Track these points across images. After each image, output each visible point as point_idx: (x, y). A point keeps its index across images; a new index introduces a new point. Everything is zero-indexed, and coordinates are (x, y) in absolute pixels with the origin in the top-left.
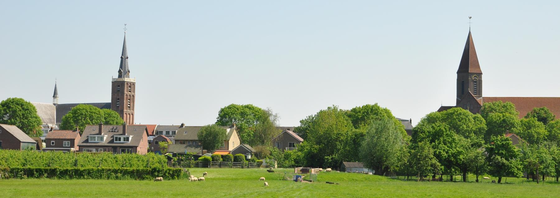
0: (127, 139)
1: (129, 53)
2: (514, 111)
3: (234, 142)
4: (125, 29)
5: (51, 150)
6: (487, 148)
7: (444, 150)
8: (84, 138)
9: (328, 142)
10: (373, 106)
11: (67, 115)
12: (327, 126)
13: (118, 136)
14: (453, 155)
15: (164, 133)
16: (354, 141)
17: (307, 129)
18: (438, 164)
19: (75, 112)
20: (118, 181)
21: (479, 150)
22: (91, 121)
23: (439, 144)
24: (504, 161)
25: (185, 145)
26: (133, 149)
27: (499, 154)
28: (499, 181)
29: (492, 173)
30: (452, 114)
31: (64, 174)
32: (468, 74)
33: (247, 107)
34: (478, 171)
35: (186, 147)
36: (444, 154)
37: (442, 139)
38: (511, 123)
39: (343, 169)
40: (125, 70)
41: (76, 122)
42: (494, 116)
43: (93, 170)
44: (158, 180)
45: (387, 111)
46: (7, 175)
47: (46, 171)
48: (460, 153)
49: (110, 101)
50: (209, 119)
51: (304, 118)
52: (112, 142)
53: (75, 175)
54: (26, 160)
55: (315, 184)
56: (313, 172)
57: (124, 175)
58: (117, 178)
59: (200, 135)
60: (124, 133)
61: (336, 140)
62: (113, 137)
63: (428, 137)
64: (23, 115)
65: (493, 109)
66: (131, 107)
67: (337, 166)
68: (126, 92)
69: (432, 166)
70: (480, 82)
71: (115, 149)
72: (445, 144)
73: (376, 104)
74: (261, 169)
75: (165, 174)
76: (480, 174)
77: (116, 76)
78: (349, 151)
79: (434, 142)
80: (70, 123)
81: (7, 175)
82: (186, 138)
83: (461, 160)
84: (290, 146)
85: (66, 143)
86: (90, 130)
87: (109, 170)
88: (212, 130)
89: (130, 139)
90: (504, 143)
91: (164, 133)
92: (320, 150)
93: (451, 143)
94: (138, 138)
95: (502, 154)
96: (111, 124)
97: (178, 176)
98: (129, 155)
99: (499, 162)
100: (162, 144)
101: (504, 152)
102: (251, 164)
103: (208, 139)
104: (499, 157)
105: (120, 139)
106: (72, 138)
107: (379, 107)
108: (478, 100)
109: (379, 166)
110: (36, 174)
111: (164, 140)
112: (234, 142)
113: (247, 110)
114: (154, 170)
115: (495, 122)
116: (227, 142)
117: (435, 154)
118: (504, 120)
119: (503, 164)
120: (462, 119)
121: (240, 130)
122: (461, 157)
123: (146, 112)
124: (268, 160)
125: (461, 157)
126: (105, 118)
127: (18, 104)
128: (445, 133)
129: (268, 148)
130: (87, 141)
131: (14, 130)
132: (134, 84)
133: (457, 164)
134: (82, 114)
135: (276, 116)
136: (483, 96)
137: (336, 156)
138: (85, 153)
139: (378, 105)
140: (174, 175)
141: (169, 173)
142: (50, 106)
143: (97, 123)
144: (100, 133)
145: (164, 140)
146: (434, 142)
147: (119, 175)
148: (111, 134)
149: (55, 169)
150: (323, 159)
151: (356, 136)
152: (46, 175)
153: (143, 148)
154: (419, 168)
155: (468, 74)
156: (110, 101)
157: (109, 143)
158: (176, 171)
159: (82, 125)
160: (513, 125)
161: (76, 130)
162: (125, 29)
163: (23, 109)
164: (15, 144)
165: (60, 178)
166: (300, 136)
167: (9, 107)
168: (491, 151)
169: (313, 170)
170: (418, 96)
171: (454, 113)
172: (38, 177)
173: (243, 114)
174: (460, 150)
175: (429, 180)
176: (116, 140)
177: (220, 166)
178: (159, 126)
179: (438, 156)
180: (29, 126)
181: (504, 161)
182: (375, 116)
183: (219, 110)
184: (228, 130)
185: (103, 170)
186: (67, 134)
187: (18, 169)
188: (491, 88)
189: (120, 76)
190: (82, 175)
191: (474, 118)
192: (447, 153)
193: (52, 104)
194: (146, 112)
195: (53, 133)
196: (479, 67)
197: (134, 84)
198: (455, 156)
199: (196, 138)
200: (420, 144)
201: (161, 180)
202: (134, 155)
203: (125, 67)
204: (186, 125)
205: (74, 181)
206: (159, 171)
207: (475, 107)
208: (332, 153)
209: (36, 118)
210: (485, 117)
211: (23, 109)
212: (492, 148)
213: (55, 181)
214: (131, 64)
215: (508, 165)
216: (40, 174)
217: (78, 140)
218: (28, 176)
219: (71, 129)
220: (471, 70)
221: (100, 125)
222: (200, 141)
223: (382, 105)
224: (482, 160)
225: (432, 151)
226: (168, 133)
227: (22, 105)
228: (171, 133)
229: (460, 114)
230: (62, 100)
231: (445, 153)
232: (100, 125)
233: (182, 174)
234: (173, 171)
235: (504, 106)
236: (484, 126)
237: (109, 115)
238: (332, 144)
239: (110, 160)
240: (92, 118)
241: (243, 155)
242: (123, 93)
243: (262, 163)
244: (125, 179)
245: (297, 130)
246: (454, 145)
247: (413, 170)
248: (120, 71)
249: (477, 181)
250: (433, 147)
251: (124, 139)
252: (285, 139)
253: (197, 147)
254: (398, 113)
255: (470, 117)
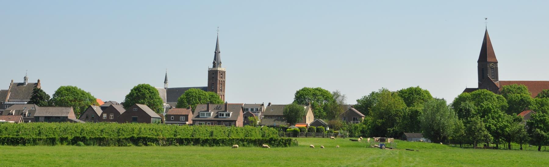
0: (229, 115)
1: (221, 49)
2: (527, 92)
3: (310, 119)
4: (218, 31)
5: (172, 123)
6: (527, 122)
7: (493, 124)
8: (196, 114)
9: (389, 117)
10: (416, 88)
11: (182, 96)
12: (386, 105)
13: (222, 113)
14: (500, 127)
15: (250, 110)
16: (411, 116)
17: (365, 106)
18: (490, 135)
19: (187, 94)
20: (245, 148)
21: (520, 124)
22: (200, 101)
23: (489, 118)
24: (543, 133)
25: (273, 120)
26: (232, 122)
27: (538, 127)
28: (539, 149)
29: (532, 143)
30: (479, 94)
31: (205, 142)
32: (486, 62)
33: (317, 89)
34: (521, 141)
35: (275, 121)
36: (493, 127)
37: (490, 115)
38: (528, 102)
39: (405, 139)
40: (218, 62)
41: (189, 102)
42: (514, 96)
43: (226, 139)
44: (264, 147)
45: (427, 92)
46: (165, 143)
47: (192, 140)
48: (506, 126)
49: (207, 86)
50: (289, 100)
51: (360, 97)
52: (217, 117)
53: (213, 143)
54: (176, 131)
55: (394, 150)
56: (389, 142)
57: (248, 144)
58: (244, 145)
59: (285, 112)
60: (226, 111)
61: (396, 115)
62: (218, 113)
63: (479, 113)
64: (150, 96)
65: (510, 90)
66: (223, 90)
67: (399, 136)
68: (218, 78)
69: (484, 136)
70: (497, 68)
71: (219, 122)
72: (493, 119)
73: (418, 87)
74: (346, 139)
75: (279, 143)
76: (523, 143)
77: (211, 66)
78: (406, 124)
79: (484, 117)
80: (184, 102)
81: (165, 143)
82: (273, 114)
83: (507, 132)
84: (354, 120)
85: (182, 118)
86: (200, 108)
87: (238, 139)
88: (294, 107)
89: (231, 114)
90: (542, 118)
91: (250, 110)
92: (383, 123)
93: (497, 118)
94: (236, 114)
95: (541, 127)
96: (214, 103)
97: (289, 144)
98: (229, 128)
99: (539, 134)
100: (250, 118)
101: (542, 126)
102: (329, 135)
103: (291, 115)
104: (538, 130)
105: (223, 115)
106: (186, 114)
107: (421, 89)
108: (496, 83)
109: (436, 135)
110: (185, 142)
111: (252, 115)
112: (310, 119)
113: (317, 92)
114: (271, 139)
115: (515, 101)
116: (305, 117)
117: (486, 127)
118: (522, 100)
119: (542, 135)
120: (488, 98)
121: (313, 107)
122: (507, 129)
123: (233, 94)
124: (342, 131)
125: (507, 129)
126: (210, 99)
127: (146, 89)
128: (493, 110)
129: (338, 121)
130: (198, 116)
131: (144, 108)
132: (224, 72)
133: (503, 135)
134: (193, 96)
135: (343, 97)
136: (500, 79)
137: (396, 128)
138: (197, 126)
139: (420, 87)
140: (286, 143)
141: (282, 142)
142: (162, 89)
143: (204, 103)
144: (208, 110)
145: (252, 115)
146: (484, 117)
147: (245, 143)
148: (217, 111)
149: (199, 139)
150: (386, 131)
151: (412, 112)
152: (192, 143)
153: (240, 122)
154: (474, 138)
155: (486, 62)
156: (207, 86)
157: (215, 117)
158: (288, 140)
159: (194, 104)
160: (529, 103)
161: (189, 108)
162: (218, 31)
163: (150, 92)
164: (147, 119)
165: (202, 145)
166: (359, 111)
167: (140, 91)
168: (530, 125)
169: (389, 139)
170: (450, 81)
171: (481, 94)
172: (186, 145)
173: (314, 95)
174: (506, 124)
175: (481, 148)
176: (220, 116)
177: (306, 136)
178: (245, 104)
179: (489, 129)
180: (154, 105)
181: (543, 133)
182: (418, 96)
183: (296, 92)
184: (305, 107)
185: (233, 139)
186: (183, 111)
187: (172, 138)
188: (506, 73)
189: (214, 66)
190: (218, 143)
191: (498, 98)
192: (495, 126)
193: (163, 88)
194: (233, 94)
195: (172, 111)
196: (494, 57)
197: (224, 72)
198: (502, 128)
199: (283, 114)
200: (472, 119)
201: (266, 147)
202: (232, 128)
203: (218, 60)
204: (272, 104)
205: (215, 148)
206: (275, 140)
207: (495, 89)
208: (393, 126)
209: (159, 99)
210: (506, 96)
211: (150, 92)
212: (532, 123)
213: (199, 148)
214: (222, 57)
215: (546, 137)
216: (188, 143)
217: (191, 117)
218: (179, 144)
219: (185, 107)
220: (489, 60)
221: (208, 104)
222: (284, 116)
223: (423, 87)
224: (524, 132)
225: (483, 124)
226: (252, 110)
227: (149, 89)
228: (254, 110)
229: (486, 94)
230: (170, 85)
231: (493, 126)
232: (208, 104)
233: (292, 143)
234: (285, 140)
235: (519, 88)
236: (505, 103)
237: (212, 96)
238: (394, 118)
239: (219, 132)
240: (200, 99)
241: (324, 128)
242: (217, 79)
243: (338, 133)
244: (249, 146)
245: (356, 107)
246: (500, 119)
247: (468, 139)
248: (214, 63)
249: (521, 149)
250: (484, 121)
251: (226, 115)
252: (350, 114)
253: (283, 121)
254: (435, 94)
255: (495, 97)
